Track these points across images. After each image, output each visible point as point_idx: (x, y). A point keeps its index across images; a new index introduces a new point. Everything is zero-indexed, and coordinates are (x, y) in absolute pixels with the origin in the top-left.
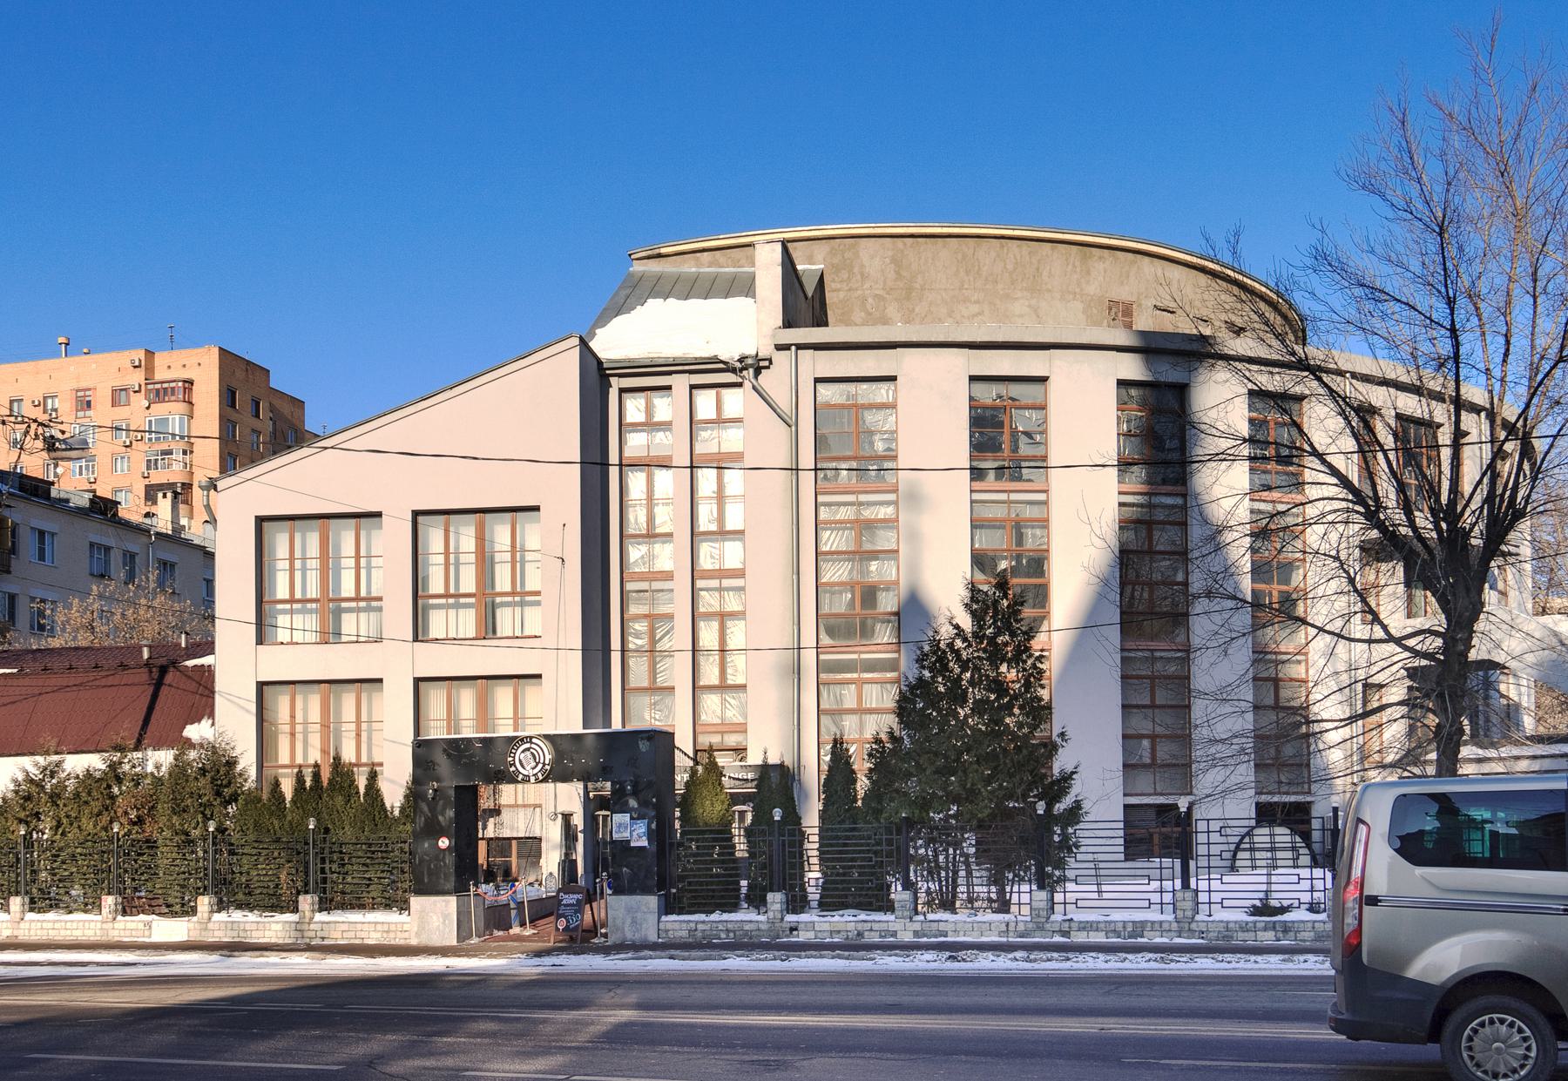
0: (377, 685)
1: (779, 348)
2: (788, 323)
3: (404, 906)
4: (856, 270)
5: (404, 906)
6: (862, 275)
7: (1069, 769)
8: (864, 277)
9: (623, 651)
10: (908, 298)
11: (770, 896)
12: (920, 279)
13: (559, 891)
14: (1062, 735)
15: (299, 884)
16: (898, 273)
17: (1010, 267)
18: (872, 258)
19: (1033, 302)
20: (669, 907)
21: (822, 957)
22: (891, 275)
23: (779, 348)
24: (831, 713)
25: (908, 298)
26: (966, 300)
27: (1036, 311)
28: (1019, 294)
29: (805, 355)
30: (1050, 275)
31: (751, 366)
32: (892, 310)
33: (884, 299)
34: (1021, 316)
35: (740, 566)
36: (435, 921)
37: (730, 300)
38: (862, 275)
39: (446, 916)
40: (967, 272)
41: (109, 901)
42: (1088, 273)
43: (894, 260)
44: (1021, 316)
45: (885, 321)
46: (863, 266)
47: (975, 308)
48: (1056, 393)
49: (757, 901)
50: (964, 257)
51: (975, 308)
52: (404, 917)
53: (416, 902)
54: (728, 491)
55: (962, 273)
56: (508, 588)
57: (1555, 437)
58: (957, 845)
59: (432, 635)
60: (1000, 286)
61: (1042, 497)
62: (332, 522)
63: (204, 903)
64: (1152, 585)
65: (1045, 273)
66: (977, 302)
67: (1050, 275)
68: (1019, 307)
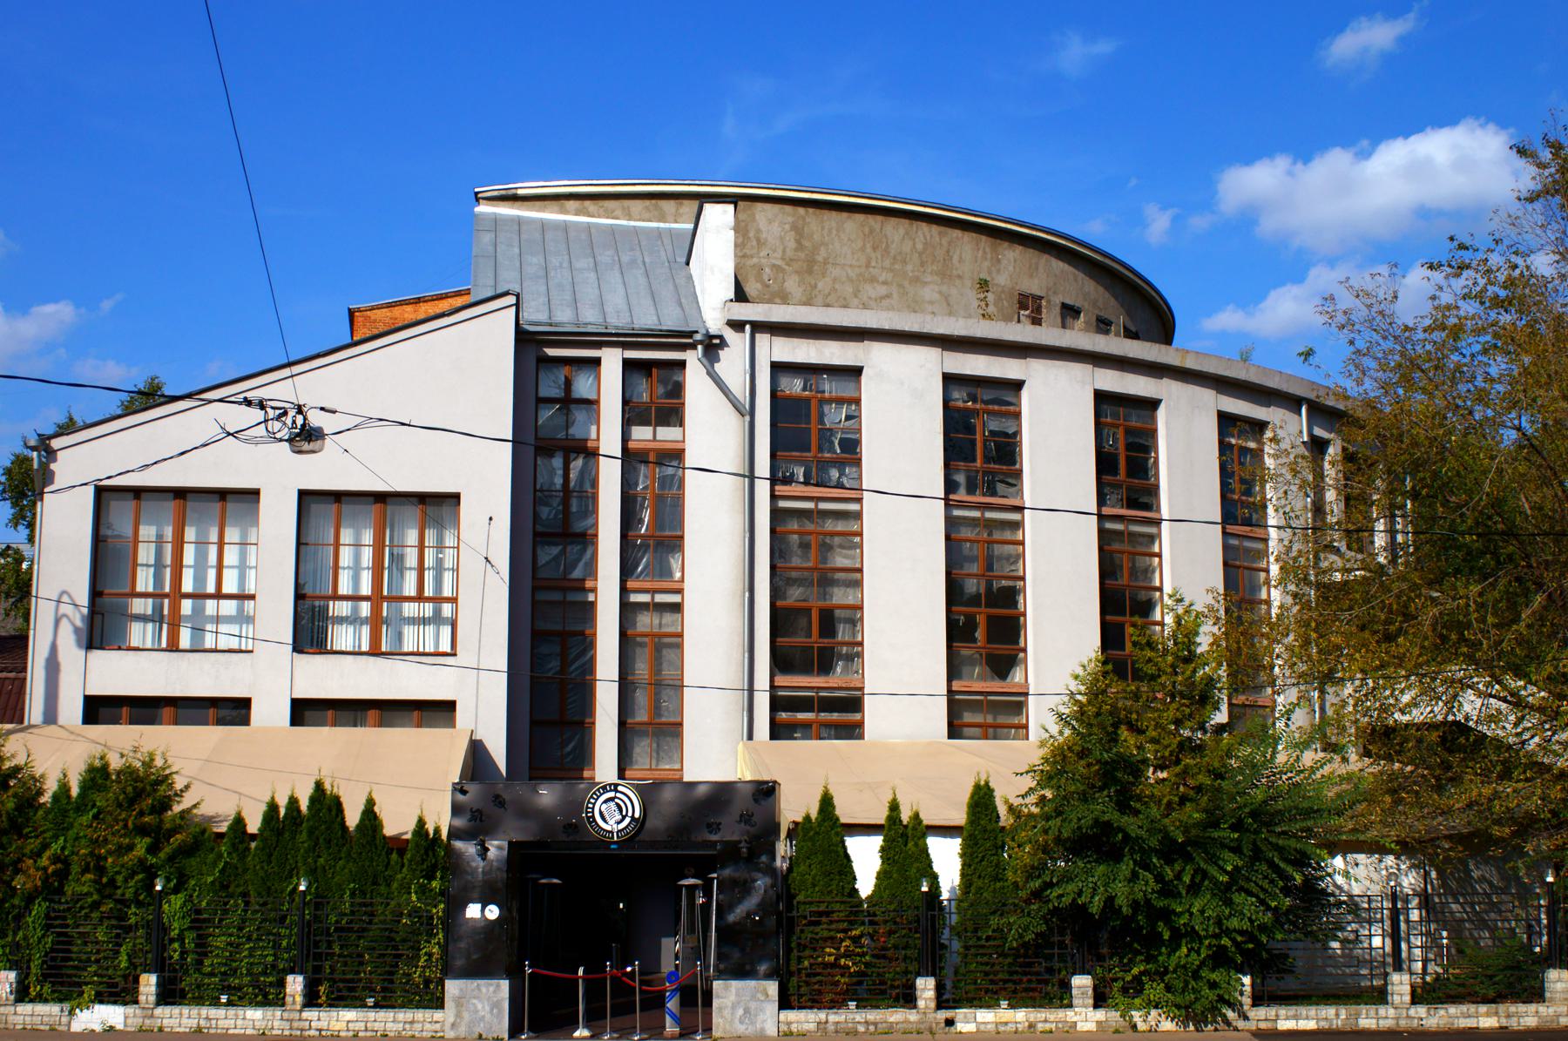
0: (446, 510)
1: (737, 326)
2: (741, 296)
3: (437, 1002)
4: (751, 235)
5: (437, 1002)
6: (758, 240)
7: (890, 797)
8: (760, 243)
9: (751, 690)
10: (810, 271)
11: (290, 978)
12: (823, 252)
13: (1386, 984)
14: (1452, 239)
15: (1356, 374)
16: (798, 242)
17: (919, 246)
18: (770, 222)
19: (944, 288)
20: (785, 1003)
21: (1157, 459)
22: (792, 244)
23: (737, 326)
24: (390, 599)
25: (810, 271)
26: (873, 280)
27: (947, 298)
28: (929, 278)
29: (763, 340)
30: (961, 260)
31: (701, 342)
32: (792, 285)
33: (783, 270)
34: (931, 302)
35: (758, 336)
36: (482, 1008)
37: (359, 731)
38: (758, 240)
39: (496, 1005)
40: (875, 249)
41: (852, 1004)
42: (999, 261)
43: (794, 227)
44: (931, 302)
45: (784, 298)
46: (759, 231)
47: (883, 290)
48: (1027, 401)
49: (123, 993)
50: (871, 231)
51: (883, 290)
52: (438, 1015)
53: (452, 987)
54: (226, 562)
55: (869, 250)
56: (413, 593)
57: (229, 434)
58: (1037, 804)
59: (133, 644)
60: (909, 267)
61: (675, 598)
62: (760, 206)
63: (1004, 1004)
64: (891, 270)
65: (956, 258)
66: (885, 283)
67: (961, 260)
68: (928, 293)
